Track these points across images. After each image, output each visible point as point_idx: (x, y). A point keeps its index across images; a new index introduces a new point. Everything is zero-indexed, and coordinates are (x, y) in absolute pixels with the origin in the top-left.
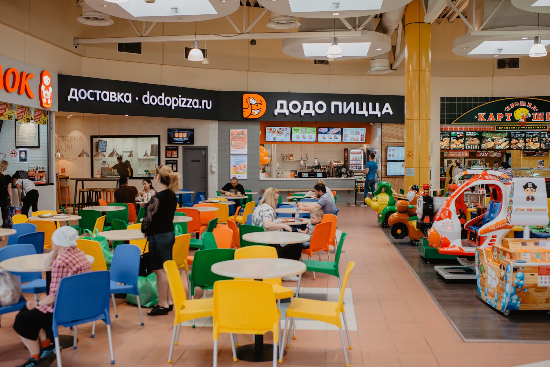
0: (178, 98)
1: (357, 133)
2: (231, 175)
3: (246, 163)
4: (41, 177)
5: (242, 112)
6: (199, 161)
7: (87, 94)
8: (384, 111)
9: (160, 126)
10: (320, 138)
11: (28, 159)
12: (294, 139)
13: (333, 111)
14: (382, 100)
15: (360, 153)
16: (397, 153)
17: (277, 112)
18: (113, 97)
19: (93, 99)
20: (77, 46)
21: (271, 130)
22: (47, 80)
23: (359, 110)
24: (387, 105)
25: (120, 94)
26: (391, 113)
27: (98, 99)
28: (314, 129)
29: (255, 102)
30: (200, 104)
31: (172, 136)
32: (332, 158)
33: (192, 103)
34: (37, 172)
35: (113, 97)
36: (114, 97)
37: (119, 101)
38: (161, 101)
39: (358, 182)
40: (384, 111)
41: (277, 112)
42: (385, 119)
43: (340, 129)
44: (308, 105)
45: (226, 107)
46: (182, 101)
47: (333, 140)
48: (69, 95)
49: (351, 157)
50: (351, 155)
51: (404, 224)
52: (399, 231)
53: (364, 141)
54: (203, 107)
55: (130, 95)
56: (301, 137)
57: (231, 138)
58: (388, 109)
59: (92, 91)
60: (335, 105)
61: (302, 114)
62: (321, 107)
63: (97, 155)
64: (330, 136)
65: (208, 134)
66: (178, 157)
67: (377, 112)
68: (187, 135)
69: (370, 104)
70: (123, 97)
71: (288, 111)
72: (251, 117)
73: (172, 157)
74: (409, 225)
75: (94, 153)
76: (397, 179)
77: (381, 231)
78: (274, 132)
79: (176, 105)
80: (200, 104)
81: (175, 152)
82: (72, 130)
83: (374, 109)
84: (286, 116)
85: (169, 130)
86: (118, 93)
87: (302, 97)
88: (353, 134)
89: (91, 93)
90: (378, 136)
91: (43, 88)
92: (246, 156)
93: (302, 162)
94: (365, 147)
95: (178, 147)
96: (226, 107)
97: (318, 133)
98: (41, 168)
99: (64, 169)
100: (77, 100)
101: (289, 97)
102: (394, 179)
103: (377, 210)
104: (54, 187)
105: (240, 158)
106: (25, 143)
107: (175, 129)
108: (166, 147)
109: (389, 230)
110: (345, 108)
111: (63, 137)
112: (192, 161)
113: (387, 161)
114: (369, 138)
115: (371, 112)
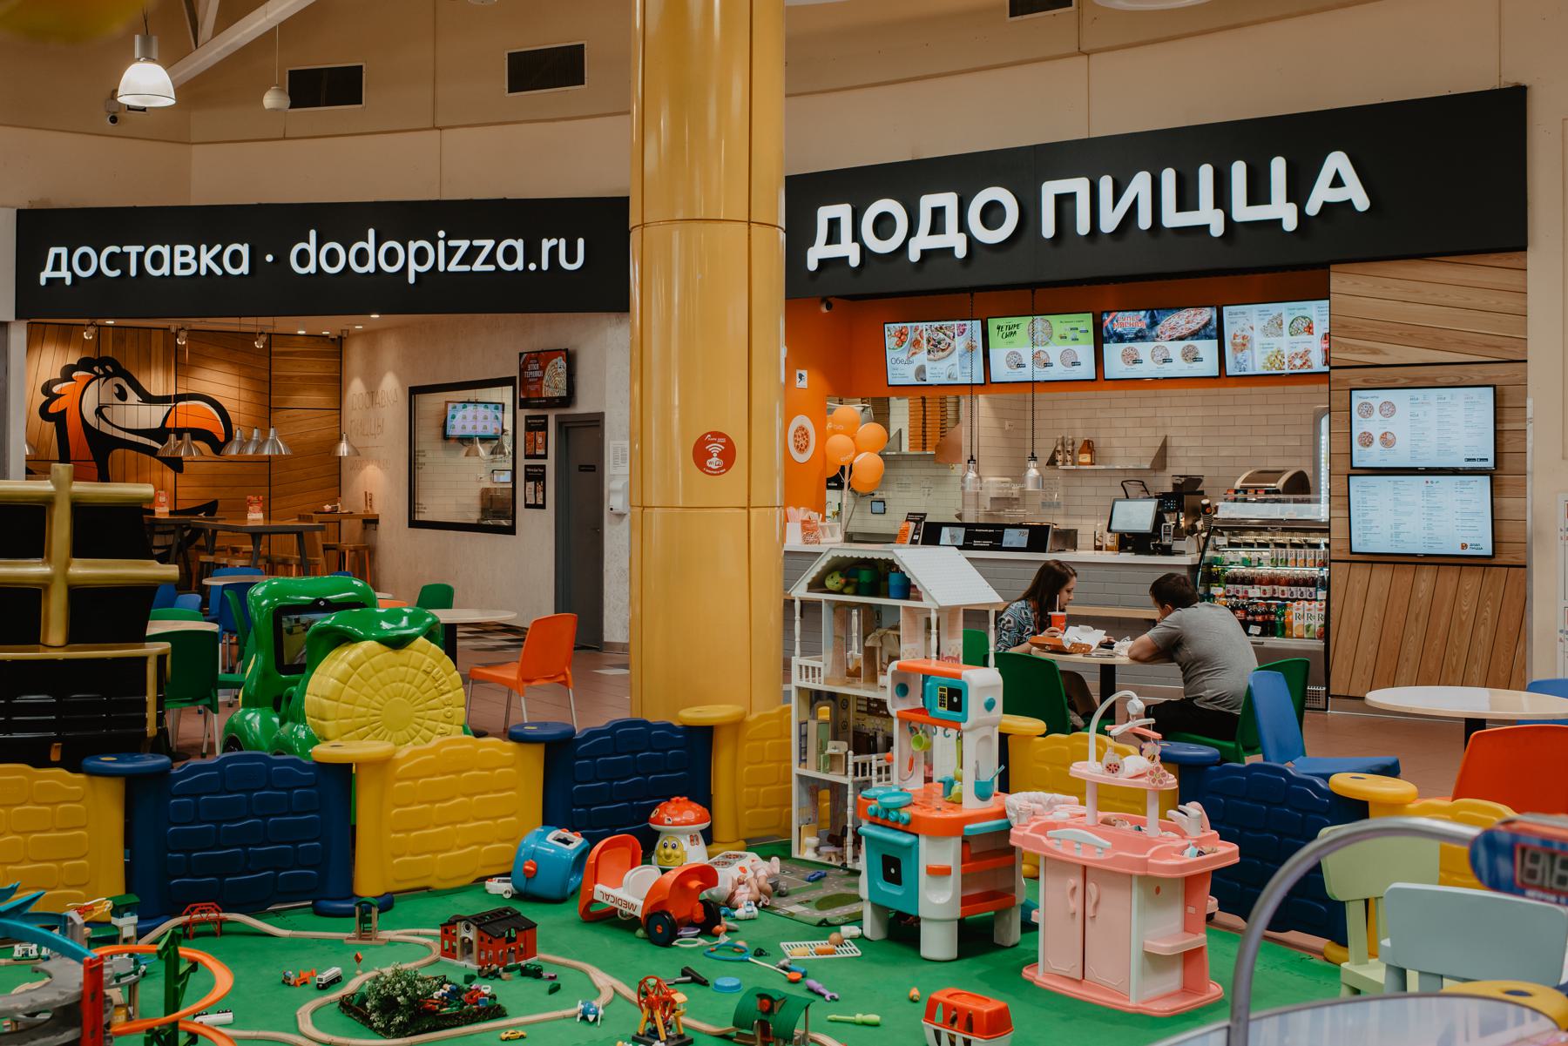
1: (1302, 325)
2: (626, 533)
8: (1321, 194)
10: (1116, 360)
12: (1001, 372)
17: (818, 252)
18: (184, 260)
19: (117, 273)
21: (902, 335)
23: (1072, 196)
24: (1337, 162)
25: (208, 250)
26: (1362, 202)
27: (133, 272)
28: (1085, 321)
30: (532, 254)
33: (500, 255)
35: (184, 260)
36: (189, 259)
37: (203, 272)
38: (362, 257)
40: (1321, 194)
43: (1207, 314)
47: (1179, 368)
54: (545, 266)
55: (244, 250)
56: (1027, 359)
59: (116, 249)
66: (545, 457)
67: (1282, 210)
69: (1239, 171)
70: (217, 259)
76: (1426, 576)
77: (1341, 898)
80: (532, 254)
83: (1258, 192)
86: (203, 248)
87: (907, 179)
97: (1101, 338)
100: (68, 282)
102: (1405, 575)
109: (776, 997)
115: (1243, 212)
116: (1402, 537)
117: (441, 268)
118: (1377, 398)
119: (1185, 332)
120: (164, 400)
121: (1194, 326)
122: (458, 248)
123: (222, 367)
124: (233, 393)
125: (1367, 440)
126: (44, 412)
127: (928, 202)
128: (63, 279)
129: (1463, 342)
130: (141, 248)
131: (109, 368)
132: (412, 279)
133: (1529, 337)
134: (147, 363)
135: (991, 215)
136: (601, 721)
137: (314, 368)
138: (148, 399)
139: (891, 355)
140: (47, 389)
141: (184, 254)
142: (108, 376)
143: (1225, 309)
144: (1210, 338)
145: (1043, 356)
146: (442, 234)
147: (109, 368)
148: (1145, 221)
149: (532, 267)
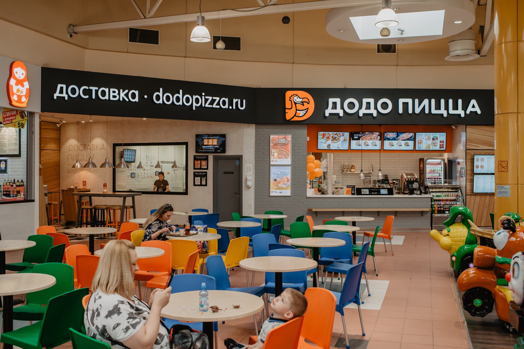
0: (201, 96)
3: (289, 177)
4: (18, 192)
5: (285, 113)
6: (233, 173)
7: (80, 92)
9: (188, 130)
10: (387, 145)
11: (8, 170)
13: (401, 111)
14: (466, 95)
15: (440, 164)
16: (486, 163)
17: (327, 113)
18: (113, 94)
19: (87, 97)
20: (74, 35)
22: (19, 72)
23: (407, 103)
24: (473, 102)
26: (479, 112)
27: (94, 97)
29: (301, 100)
30: (231, 103)
31: (200, 144)
32: (401, 170)
33: (220, 103)
34: (14, 186)
35: (113, 94)
37: (121, 99)
38: (178, 99)
39: (435, 200)
40: (470, 109)
41: (327, 113)
42: (472, 120)
43: (412, 134)
44: (368, 104)
45: (265, 107)
46: (206, 100)
47: (404, 148)
48: (55, 92)
49: (428, 168)
50: (427, 166)
51: (490, 292)
52: (478, 302)
53: (444, 149)
54: (234, 108)
55: (137, 93)
57: (271, 145)
58: (474, 107)
59: (87, 88)
60: (403, 103)
61: (361, 115)
62: (385, 106)
63: (120, 165)
64: (400, 143)
65: (243, 140)
66: (207, 169)
67: (460, 112)
68: (218, 142)
69: (451, 101)
70: (127, 95)
71: (342, 111)
72: (295, 119)
73: (201, 169)
74: (496, 293)
75: (117, 162)
78: (328, 138)
80: (231, 103)
81: (204, 163)
82: (94, 138)
83: (455, 107)
84: (340, 117)
85: (198, 136)
86: (121, 90)
87: (360, 94)
88: (427, 140)
89: (84, 90)
90: (462, 142)
91: (12, 82)
92: (289, 168)
93: (362, 175)
94: (446, 156)
95: (207, 156)
96: (265, 107)
98: (20, 181)
99: (85, 182)
100: (66, 98)
101: (343, 93)
102: (483, 198)
103: (448, 249)
104: (36, 205)
105: (282, 169)
106: (5, 151)
107: (203, 135)
108: (195, 156)
110: (416, 107)
111: (85, 145)
112: (225, 173)
113: (473, 174)
114: (450, 146)
115: (451, 112)
117: (203, 105)
118: (480, 157)
121: (408, 137)
122: (216, 100)
125: (477, 167)
127: (365, 101)
128: (64, 97)
130: (97, 88)
143: (417, 134)
148: (427, 111)
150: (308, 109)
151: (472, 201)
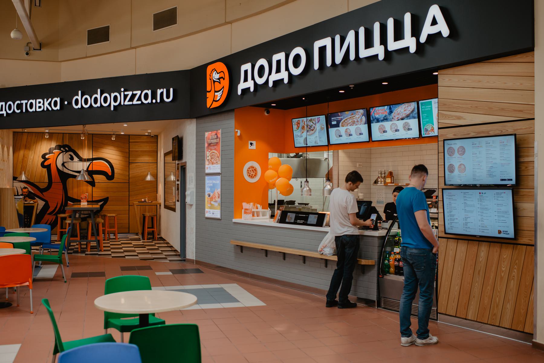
17: (242, 86)
18: (40, 105)
19: (19, 111)
27: (24, 111)
30: (154, 96)
33: (142, 96)
35: (40, 105)
36: (41, 105)
37: (45, 109)
40: (427, 30)
43: (413, 105)
46: (126, 97)
47: (403, 134)
54: (159, 101)
55: (58, 100)
67: (409, 42)
79: (116, 104)
80: (154, 96)
86: (45, 100)
87: (266, 49)
89: (18, 104)
100: (5, 115)
115: (393, 46)
116: (469, 225)
117: (122, 104)
119: (404, 115)
120: (88, 160)
121: (408, 112)
123: (110, 148)
124: (114, 157)
126: (43, 165)
129: (503, 109)
131: (67, 149)
132: (112, 109)
133: (535, 104)
134: (81, 145)
135: (297, 60)
136: (353, 275)
137: (146, 147)
138: (81, 159)
139: (295, 133)
140: (44, 156)
141: (40, 102)
142: (66, 151)
143: (420, 102)
144: (414, 118)
145: (348, 131)
146: (122, 89)
147: (67, 149)
149: (154, 101)
150: (223, 87)
151: (451, 253)
